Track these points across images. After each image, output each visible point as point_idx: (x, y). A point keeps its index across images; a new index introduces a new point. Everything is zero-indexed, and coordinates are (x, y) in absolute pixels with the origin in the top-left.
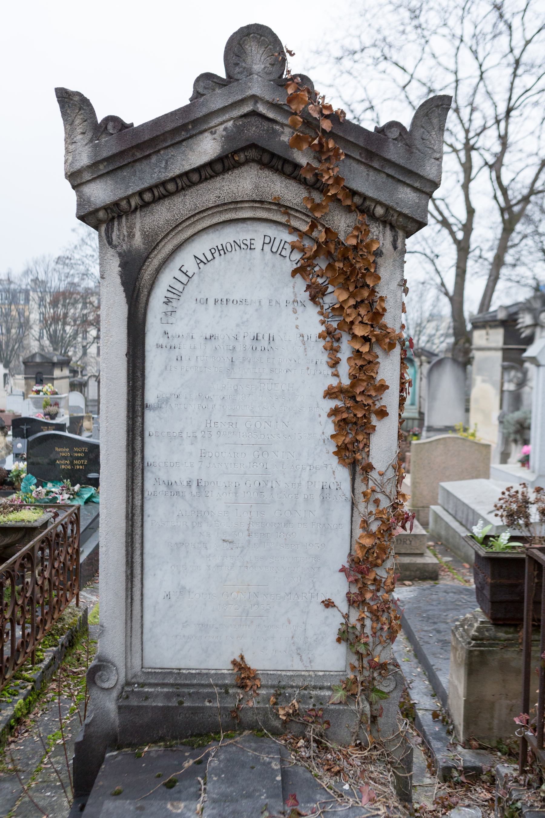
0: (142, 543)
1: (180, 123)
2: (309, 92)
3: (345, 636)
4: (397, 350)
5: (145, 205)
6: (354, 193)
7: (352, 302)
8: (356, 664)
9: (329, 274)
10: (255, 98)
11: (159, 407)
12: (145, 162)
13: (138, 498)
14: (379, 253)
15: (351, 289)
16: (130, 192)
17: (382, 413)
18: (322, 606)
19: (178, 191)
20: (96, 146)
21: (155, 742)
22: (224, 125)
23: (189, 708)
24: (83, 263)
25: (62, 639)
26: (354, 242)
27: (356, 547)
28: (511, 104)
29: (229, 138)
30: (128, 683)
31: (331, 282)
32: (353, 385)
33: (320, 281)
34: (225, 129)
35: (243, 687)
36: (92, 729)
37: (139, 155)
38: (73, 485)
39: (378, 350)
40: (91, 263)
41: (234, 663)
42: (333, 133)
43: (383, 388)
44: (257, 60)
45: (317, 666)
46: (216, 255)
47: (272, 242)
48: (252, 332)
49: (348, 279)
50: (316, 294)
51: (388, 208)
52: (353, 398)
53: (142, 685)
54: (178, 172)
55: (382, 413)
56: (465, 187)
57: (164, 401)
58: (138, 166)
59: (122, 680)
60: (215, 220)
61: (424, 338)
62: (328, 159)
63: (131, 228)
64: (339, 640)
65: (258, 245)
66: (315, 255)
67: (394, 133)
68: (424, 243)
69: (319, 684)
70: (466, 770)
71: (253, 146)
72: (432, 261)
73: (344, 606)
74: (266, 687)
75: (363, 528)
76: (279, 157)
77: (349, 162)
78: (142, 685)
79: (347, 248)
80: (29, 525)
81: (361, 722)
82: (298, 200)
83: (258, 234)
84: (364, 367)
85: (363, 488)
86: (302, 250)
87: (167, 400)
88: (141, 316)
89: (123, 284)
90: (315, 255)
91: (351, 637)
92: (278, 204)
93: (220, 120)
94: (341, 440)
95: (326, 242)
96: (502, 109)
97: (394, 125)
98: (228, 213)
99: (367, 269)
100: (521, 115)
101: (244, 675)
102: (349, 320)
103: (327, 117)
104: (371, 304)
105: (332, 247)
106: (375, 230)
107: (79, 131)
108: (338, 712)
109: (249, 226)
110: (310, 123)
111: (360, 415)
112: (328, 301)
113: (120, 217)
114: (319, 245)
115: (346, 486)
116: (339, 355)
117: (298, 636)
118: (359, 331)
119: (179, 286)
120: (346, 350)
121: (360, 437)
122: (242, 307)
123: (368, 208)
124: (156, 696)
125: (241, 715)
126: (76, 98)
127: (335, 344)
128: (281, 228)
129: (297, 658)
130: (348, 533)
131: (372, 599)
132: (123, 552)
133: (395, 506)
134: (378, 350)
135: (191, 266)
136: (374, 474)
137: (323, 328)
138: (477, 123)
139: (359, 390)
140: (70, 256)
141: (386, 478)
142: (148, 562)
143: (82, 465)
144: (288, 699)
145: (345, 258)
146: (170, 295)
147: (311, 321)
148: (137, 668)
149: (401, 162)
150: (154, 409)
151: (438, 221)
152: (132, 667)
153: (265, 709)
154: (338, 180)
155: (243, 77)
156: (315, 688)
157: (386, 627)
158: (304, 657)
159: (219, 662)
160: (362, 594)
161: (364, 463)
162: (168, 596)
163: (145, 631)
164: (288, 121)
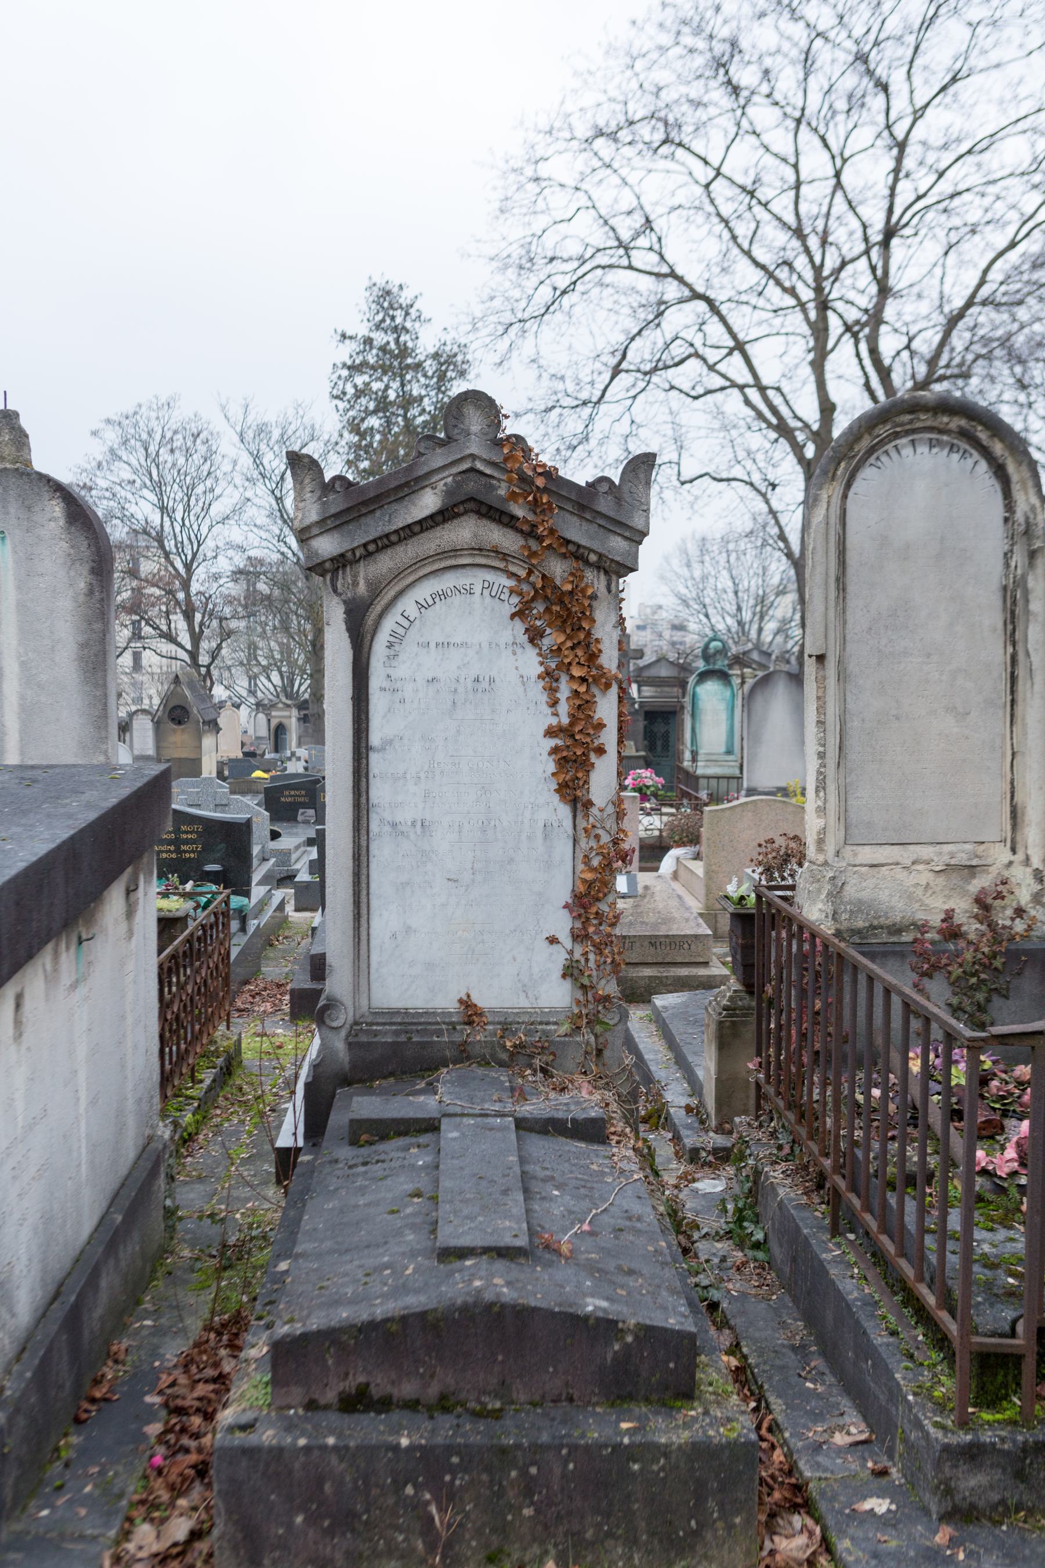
0: (368, 883)
1: (403, 481)
3: (571, 971)
4: (614, 689)
5: (369, 554)
6: (568, 542)
7: (569, 644)
8: (581, 998)
9: (547, 617)
10: (473, 457)
11: (382, 749)
12: (370, 516)
13: (364, 838)
14: (594, 597)
16: (356, 544)
17: (601, 751)
18: (547, 943)
20: (324, 503)
21: (385, 1077)
22: (445, 480)
23: (418, 1043)
24: (114, 495)
25: (220, 1061)
26: (568, 587)
27: (578, 882)
28: (894, 219)
29: (449, 493)
30: (356, 1023)
31: (549, 625)
32: (572, 724)
33: (538, 623)
34: (445, 484)
35: (470, 1023)
36: (321, 1069)
37: (364, 510)
38: (183, 882)
39: (595, 690)
40: (129, 496)
41: (461, 1001)
42: (549, 489)
43: (600, 726)
44: (475, 421)
45: (542, 1003)
46: (437, 599)
47: (490, 586)
48: (473, 673)
49: (564, 622)
50: (534, 636)
51: (600, 556)
52: (572, 736)
53: (372, 1024)
54: (401, 525)
55: (601, 751)
56: (818, 366)
57: (387, 743)
58: (363, 520)
60: (436, 567)
61: (770, 626)
62: (543, 511)
63: (355, 576)
64: (564, 976)
65: (477, 589)
66: (533, 599)
67: (604, 488)
68: (749, 464)
69: (545, 1020)
70: (715, 1151)
71: (472, 499)
72: (764, 496)
73: (568, 942)
75: (585, 863)
76: (497, 510)
77: (562, 513)
78: (372, 1024)
79: (563, 593)
80: (171, 915)
81: (586, 1053)
82: (516, 547)
83: (477, 579)
84: (583, 706)
85: (584, 824)
86: (520, 594)
87: (390, 742)
88: (364, 660)
89: (348, 630)
90: (533, 599)
91: (576, 972)
92: (497, 552)
93: (441, 476)
95: (543, 587)
96: (877, 223)
97: (604, 479)
98: (449, 560)
99: (583, 613)
102: (567, 661)
103: (540, 474)
104: (588, 646)
105: (549, 591)
106: (590, 575)
107: (308, 489)
108: (563, 1043)
109: (469, 571)
110: (523, 479)
111: (579, 753)
112: (546, 642)
113: (344, 566)
114: (536, 591)
115: (568, 823)
116: (558, 695)
117: (526, 975)
118: (577, 672)
120: (564, 690)
121: (580, 775)
122: (463, 650)
123: (582, 555)
124: (386, 1033)
125: (469, 1048)
126: (306, 460)
127: (554, 685)
129: (522, 996)
131: (595, 933)
132: (350, 891)
133: (616, 842)
134: (595, 690)
135: (412, 611)
136: (594, 811)
137: (542, 669)
138: (831, 262)
139: (577, 729)
140: (89, 484)
141: (605, 814)
142: (374, 903)
144: (514, 1033)
145: (561, 602)
146: (392, 639)
147: (531, 663)
149: (611, 514)
151: (770, 425)
152: (360, 1007)
153: (492, 1042)
154: (552, 531)
155: (461, 437)
156: (541, 1023)
157: (609, 960)
158: (530, 995)
159: (445, 1001)
160: (585, 928)
161: (584, 799)
162: (394, 936)
163: (372, 971)
164: (504, 477)
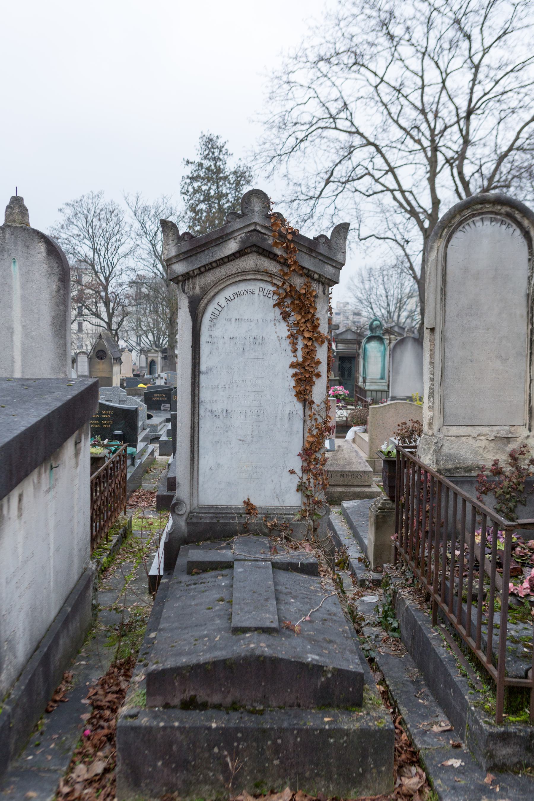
1: (220, 235)
2: (281, 221)
3: (301, 488)
4: (326, 344)
5: (201, 273)
6: (303, 268)
7: (303, 320)
8: (306, 502)
9: (292, 306)
11: (207, 373)
13: (196, 418)
14: (316, 297)
15: (303, 314)
17: (318, 375)
19: (217, 266)
20: (179, 246)
21: (205, 540)
22: (241, 235)
23: (223, 523)
24: (70, 242)
25: (121, 531)
26: (303, 291)
27: (306, 443)
28: (472, 105)
29: (243, 242)
30: (191, 512)
32: (304, 361)
33: (287, 309)
34: (241, 238)
35: (249, 513)
36: (173, 536)
37: (199, 251)
38: (103, 440)
39: (316, 344)
40: (77, 243)
41: (245, 502)
42: (294, 240)
43: (318, 363)
44: (257, 205)
46: (236, 297)
47: (263, 290)
48: (254, 335)
49: (301, 309)
50: (285, 316)
51: (320, 275)
52: (304, 368)
54: (218, 258)
55: (318, 375)
56: (432, 180)
58: (199, 255)
59: (188, 511)
60: (236, 280)
61: (404, 314)
63: (194, 284)
64: (298, 490)
65: (257, 292)
66: (285, 297)
67: (322, 240)
68: (395, 230)
70: (373, 581)
71: (255, 245)
72: (402, 247)
73: (300, 473)
74: (261, 514)
75: (309, 433)
76: (267, 251)
77: (301, 253)
78: (199, 513)
79: (300, 294)
80: (97, 456)
81: (309, 530)
82: (277, 270)
83: (256, 286)
84: (309, 352)
85: (309, 413)
86: (278, 294)
87: (211, 369)
88: (198, 327)
89: (190, 311)
90: (285, 297)
92: (267, 273)
94: (298, 389)
95: (290, 291)
98: (242, 277)
99: (310, 304)
100: (483, 113)
101: (249, 508)
102: (302, 329)
103: (290, 233)
104: (313, 322)
105: (293, 293)
106: (314, 285)
107: (171, 239)
109: (252, 283)
110: (281, 235)
112: (291, 319)
113: (189, 279)
114: (287, 293)
115: (301, 412)
116: (297, 347)
118: (307, 335)
119: (217, 312)
120: (300, 345)
121: (307, 388)
122: (248, 323)
123: (311, 275)
124: (206, 518)
125: (248, 526)
126: (170, 224)
127: (295, 341)
128: (268, 283)
129: (276, 500)
130: (302, 436)
131: (314, 468)
133: (325, 422)
134: (316, 344)
135: (223, 302)
136: (314, 406)
137: (289, 333)
138: (439, 127)
140: (57, 236)
141: (320, 408)
142: (201, 451)
143: (108, 424)
144: (272, 519)
145: (299, 299)
146: (212, 317)
147: (283, 330)
148: (196, 505)
149: (326, 254)
150: (204, 374)
151: (406, 211)
153: (260, 523)
154: (295, 262)
156: (285, 514)
157: (321, 483)
158: (280, 500)
160: (308, 466)
162: (211, 468)
164: (271, 234)
